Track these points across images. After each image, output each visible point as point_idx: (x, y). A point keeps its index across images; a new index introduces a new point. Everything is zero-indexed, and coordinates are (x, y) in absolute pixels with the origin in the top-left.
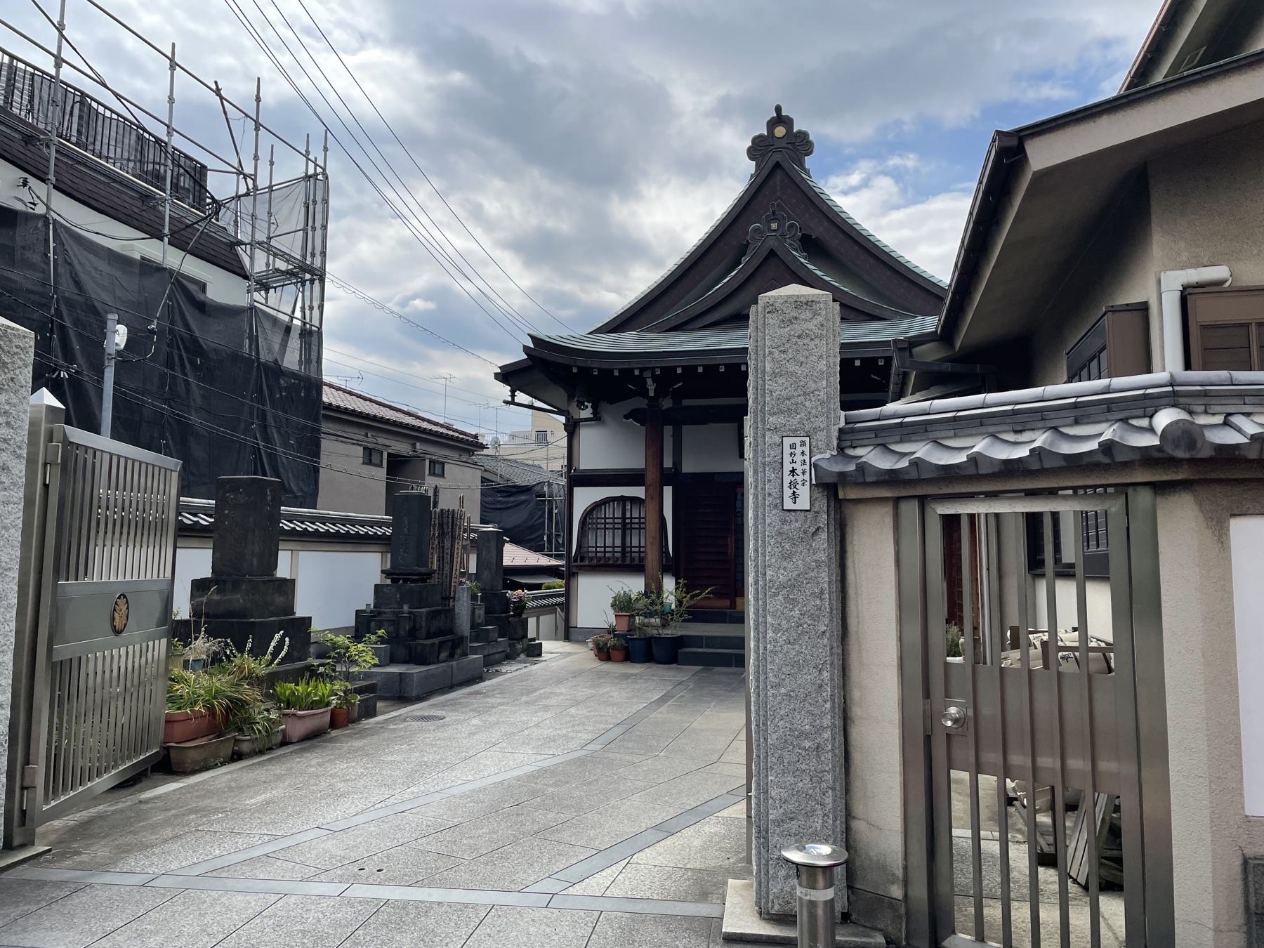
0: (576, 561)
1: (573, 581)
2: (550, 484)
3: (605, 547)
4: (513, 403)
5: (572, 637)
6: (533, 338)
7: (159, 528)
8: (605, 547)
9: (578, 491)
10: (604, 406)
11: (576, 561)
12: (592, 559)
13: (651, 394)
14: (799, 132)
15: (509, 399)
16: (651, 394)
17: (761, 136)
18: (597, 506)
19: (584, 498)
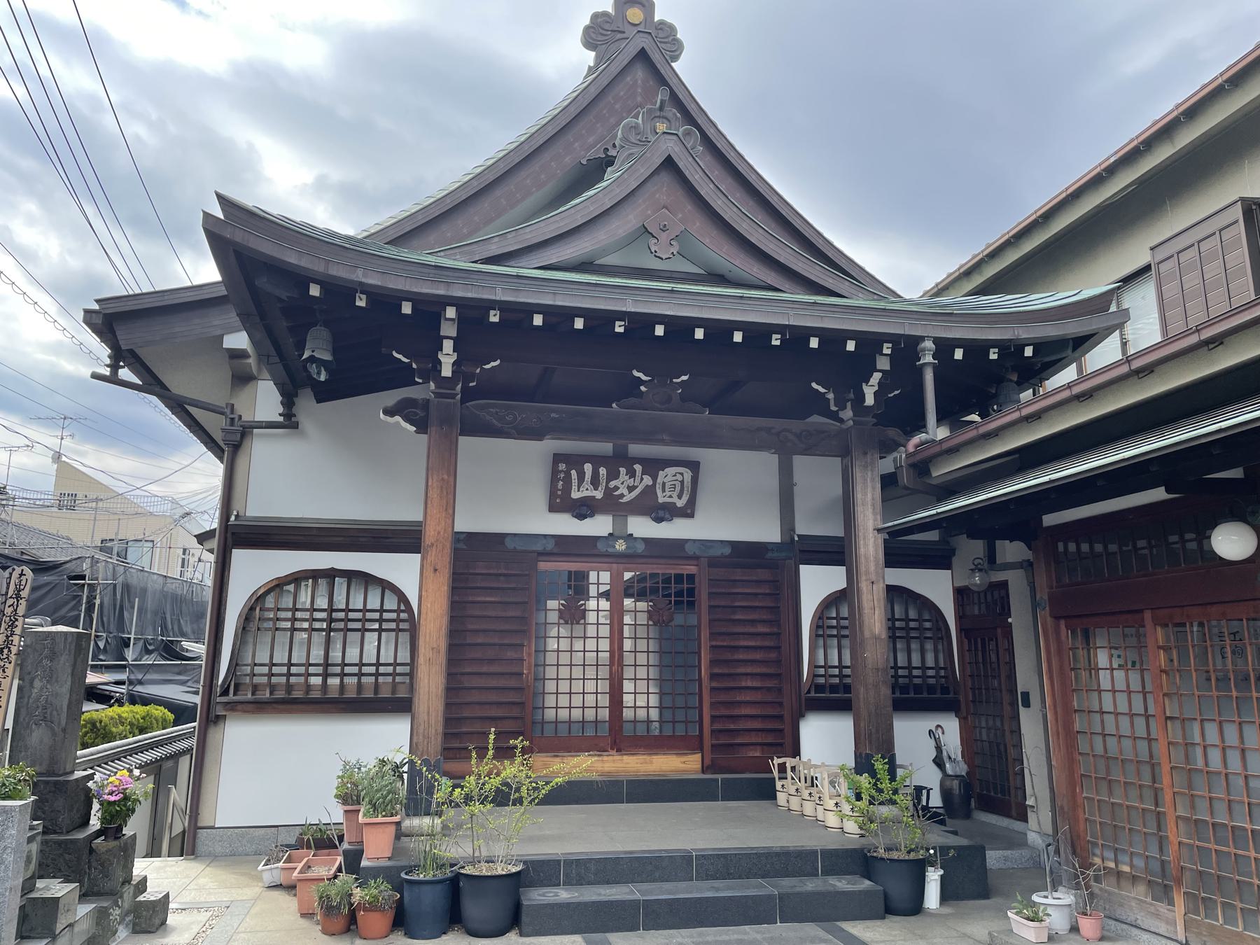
0: (225, 692)
1: (213, 733)
2: (95, 561)
3: (290, 665)
4: (113, 379)
5: (201, 848)
6: (97, 301)
7: (728, 656)
8: (290, 665)
9: (241, 558)
10: (306, 405)
11: (225, 692)
12: (255, 688)
13: (447, 371)
14: (662, 23)
15: (107, 372)
16: (447, 371)
17: (605, 14)
18: (278, 586)
19: (254, 569)
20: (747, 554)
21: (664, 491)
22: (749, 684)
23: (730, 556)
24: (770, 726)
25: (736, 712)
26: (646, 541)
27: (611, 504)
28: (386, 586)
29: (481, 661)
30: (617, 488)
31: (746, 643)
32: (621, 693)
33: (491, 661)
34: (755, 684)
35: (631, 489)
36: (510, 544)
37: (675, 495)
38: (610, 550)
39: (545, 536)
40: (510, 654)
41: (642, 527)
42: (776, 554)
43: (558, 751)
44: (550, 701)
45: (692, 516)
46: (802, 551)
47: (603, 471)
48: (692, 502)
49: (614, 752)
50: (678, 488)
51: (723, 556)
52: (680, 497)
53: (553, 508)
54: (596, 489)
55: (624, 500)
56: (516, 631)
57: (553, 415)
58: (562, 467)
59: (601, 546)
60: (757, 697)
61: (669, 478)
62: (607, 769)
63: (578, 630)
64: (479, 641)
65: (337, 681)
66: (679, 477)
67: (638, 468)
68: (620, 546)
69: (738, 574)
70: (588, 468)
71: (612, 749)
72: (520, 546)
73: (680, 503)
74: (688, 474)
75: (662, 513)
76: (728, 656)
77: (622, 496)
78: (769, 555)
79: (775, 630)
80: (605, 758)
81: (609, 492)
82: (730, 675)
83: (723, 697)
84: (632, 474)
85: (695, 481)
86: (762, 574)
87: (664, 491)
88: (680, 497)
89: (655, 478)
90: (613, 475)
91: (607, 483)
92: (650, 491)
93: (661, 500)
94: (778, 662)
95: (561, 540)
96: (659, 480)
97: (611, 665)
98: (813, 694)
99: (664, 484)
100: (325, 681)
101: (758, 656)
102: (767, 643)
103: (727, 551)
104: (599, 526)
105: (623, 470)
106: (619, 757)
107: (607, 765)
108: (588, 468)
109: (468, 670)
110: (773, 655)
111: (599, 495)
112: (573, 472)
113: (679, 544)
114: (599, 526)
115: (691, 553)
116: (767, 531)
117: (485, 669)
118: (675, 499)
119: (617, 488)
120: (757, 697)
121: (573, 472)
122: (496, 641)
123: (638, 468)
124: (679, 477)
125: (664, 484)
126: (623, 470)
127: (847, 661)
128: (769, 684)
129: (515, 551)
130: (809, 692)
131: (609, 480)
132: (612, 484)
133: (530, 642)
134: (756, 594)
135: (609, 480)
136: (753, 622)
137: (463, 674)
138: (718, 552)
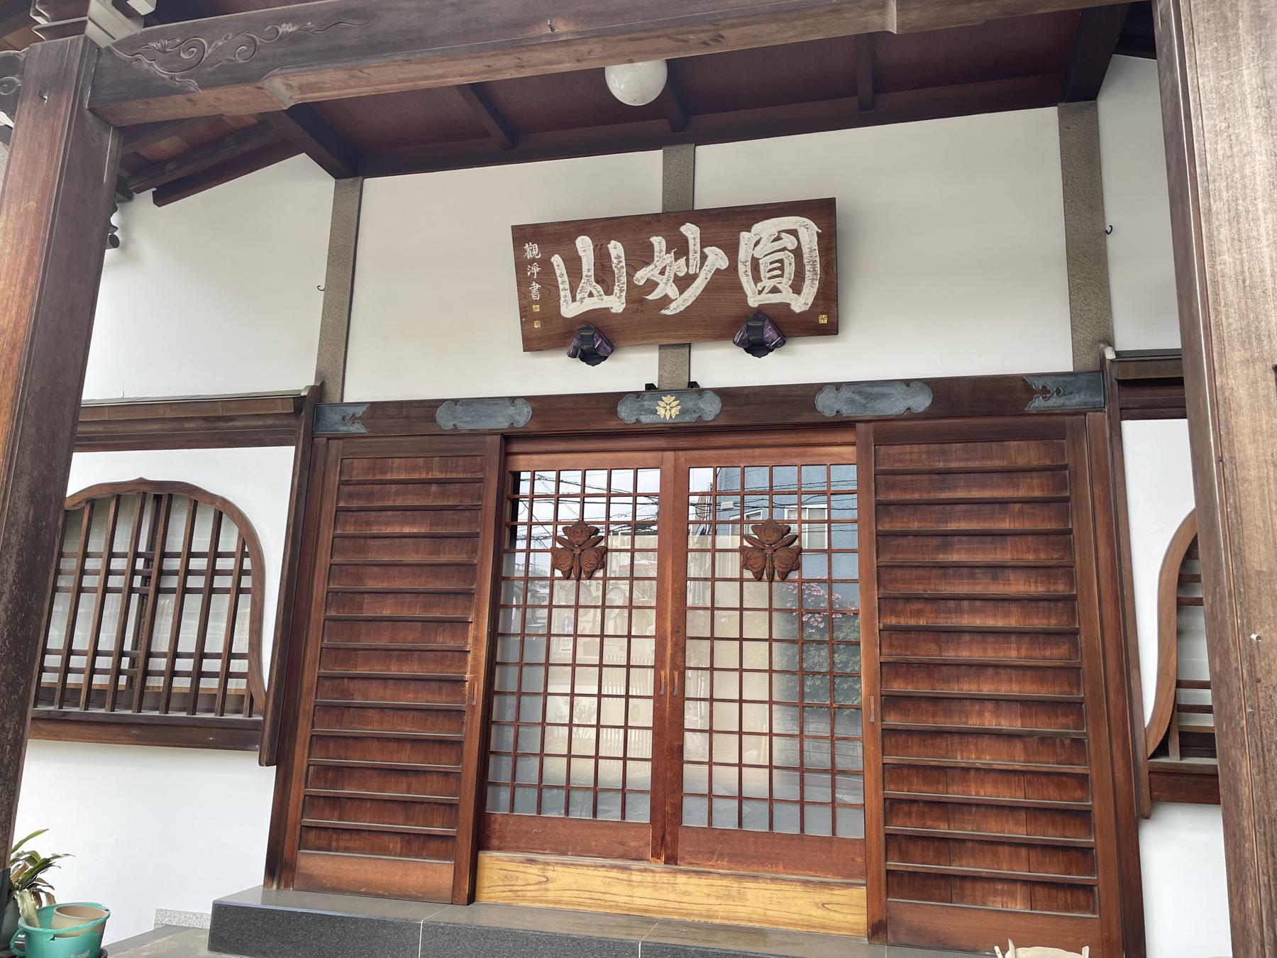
20: (976, 408)
21: (757, 278)
22: (989, 721)
23: (927, 415)
24: (1053, 837)
25: (955, 793)
26: (727, 395)
27: (645, 322)
28: (224, 511)
29: (387, 653)
30: (652, 285)
31: (978, 622)
32: (680, 729)
33: (405, 654)
34: (1005, 724)
35: (683, 283)
36: (445, 421)
37: (785, 284)
38: (646, 419)
39: (513, 399)
40: (444, 640)
41: (723, 366)
42: (1054, 402)
43: (541, 849)
44: (556, 740)
45: (831, 330)
46: (1123, 383)
47: (616, 249)
48: (829, 296)
49: (659, 865)
50: (790, 269)
51: (910, 416)
52: (797, 288)
53: (532, 343)
54: (609, 292)
55: (671, 311)
56: (456, 593)
57: (287, 28)
58: (532, 250)
59: (627, 413)
60: (1016, 759)
61: (766, 246)
62: (638, 902)
63: (592, 590)
64: (387, 612)
65: (214, 684)
66: (789, 242)
67: (690, 231)
68: (668, 410)
69: (957, 456)
70: (584, 245)
71: (656, 855)
72: (466, 423)
73: (800, 303)
74: (808, 231)
75: (762, 332)
76: (927, 651)
77: (666, 301)
78: (1038, 403)
79: (1061, 588)
80: (636, 877)
81: (637, 296)
82: (935, 700)
83: (917, 755)
84: (679, 247)
85: (829, 243)
86: (1025, 453)
87: (757, 278)
88: (797, 288)
89: (732, 250)
90: (640, 256)
91: (630, 276)
92: (726, 282)
93: (754, 301)
94: (1071, 673)
95: (542, 405)
96: (744, 254)
97: (658, 667)
98: (1174, 758)
99: (755, 263)
100: (196, 683)
101: (1012, 653)
102: (1038, 623)
103: (922, 402)
104: (629, 370)
105: (658, 242)
106: (666, 878)
107: (640, 892)
108: (584, 245)
109: (362, 670)
110: (1055, 654)
111: (616, 303)
112: (557, 260)
113: (804, 395)
114: (629, 370)
115: (829, 414)
116: (1029, 342)
117: (394, 670)
118: (786, 296)
119: (652, 285)
120: (1016, 759)
121: (557, 260)
122: (418, 613)
123: (690, 231)
124: (789, 242)
125: (755, 263)
126: (658, 242)
127: (1201, 665)
128: (1045, 726)
129: (456, 434)
130: (1162, 749)
131: (632, 269)
132: (642, 276)
133: (478, 615)
134: (1004, 503)
135: (632, 269)
136: (996, 569)
137: (352, 678)
138: (895, 406)
